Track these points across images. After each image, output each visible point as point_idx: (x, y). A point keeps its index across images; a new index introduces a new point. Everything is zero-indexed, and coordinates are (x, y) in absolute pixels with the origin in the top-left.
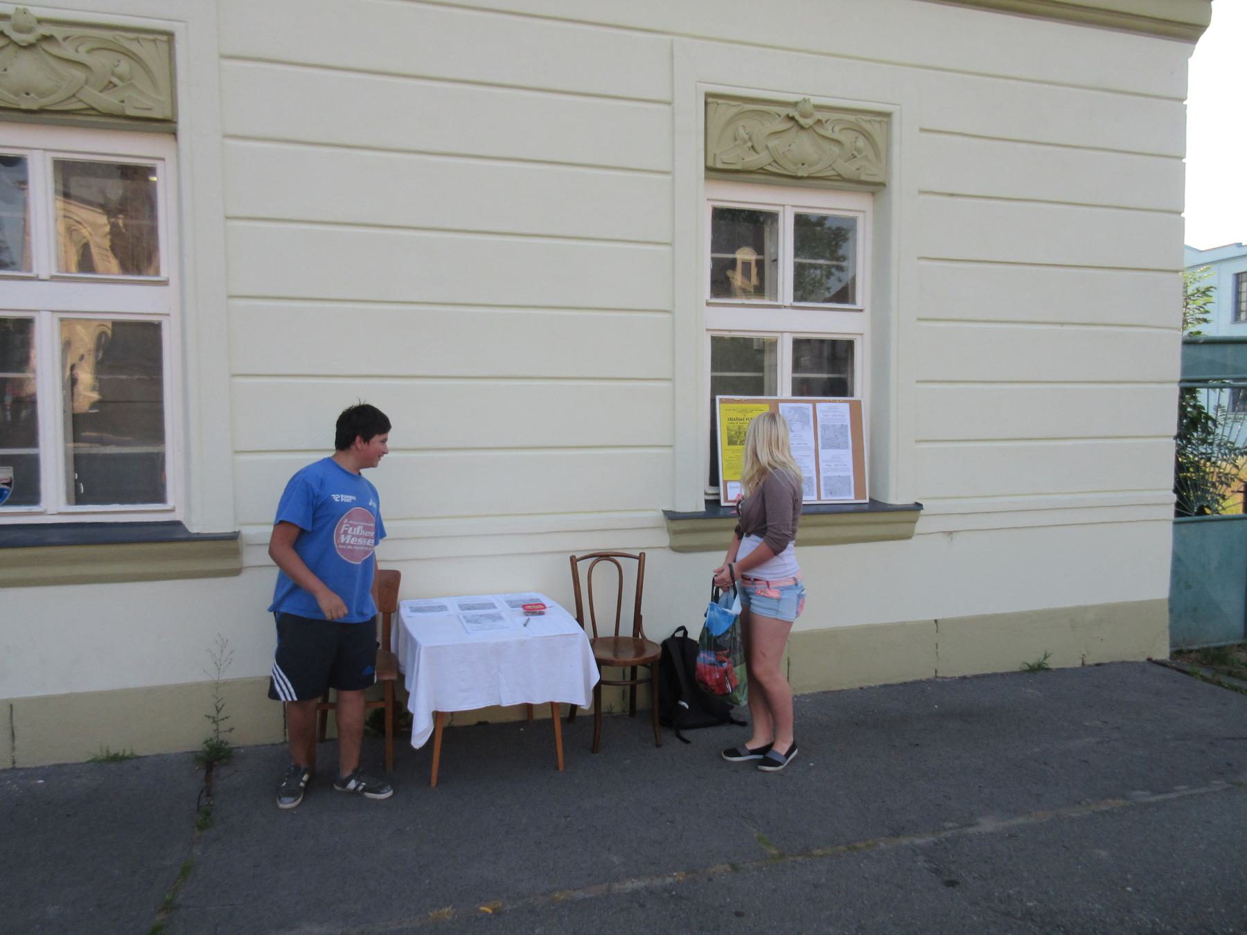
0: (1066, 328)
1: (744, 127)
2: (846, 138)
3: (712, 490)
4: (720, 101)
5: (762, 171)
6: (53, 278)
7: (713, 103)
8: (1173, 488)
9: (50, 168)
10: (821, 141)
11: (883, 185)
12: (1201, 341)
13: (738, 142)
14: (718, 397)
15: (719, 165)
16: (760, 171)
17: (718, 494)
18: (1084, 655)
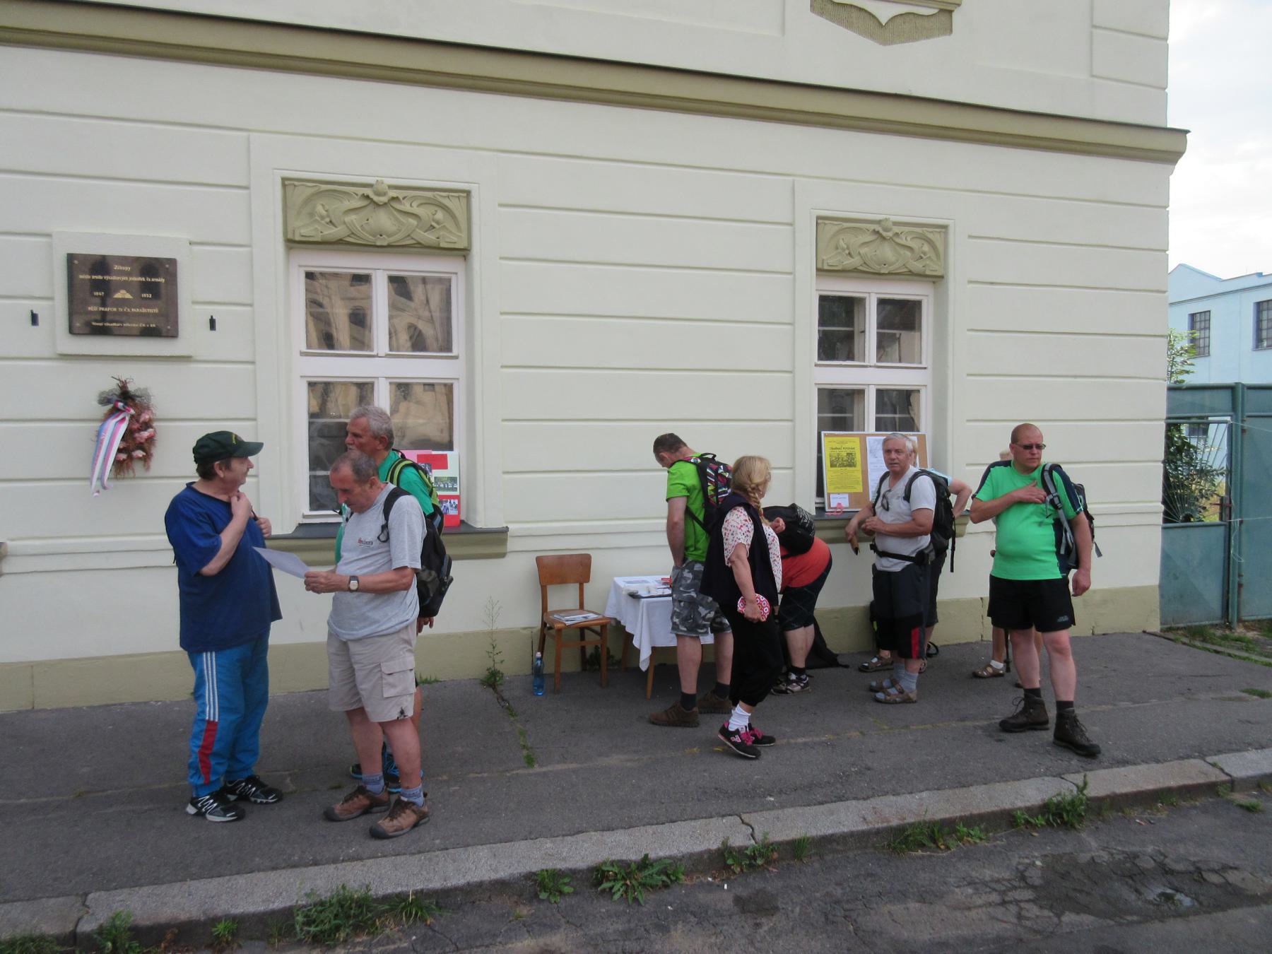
0: (1079, 380)
1: (323, 205)
2: (915, 244)
3: (819, 500)
4: (827, 222)
5: (855, 270)
6: (387, 356)
7: (290, 185)
8: (1161, 500)
9: (386, 280)
10: (898, 248)
11: (942, 277)
12: (1184, 387)
13: (839, 250)
14: (823, 433)
15: (826, 267)
16: (416, 246)
17: (824, 503)
18: (1094, 627)
